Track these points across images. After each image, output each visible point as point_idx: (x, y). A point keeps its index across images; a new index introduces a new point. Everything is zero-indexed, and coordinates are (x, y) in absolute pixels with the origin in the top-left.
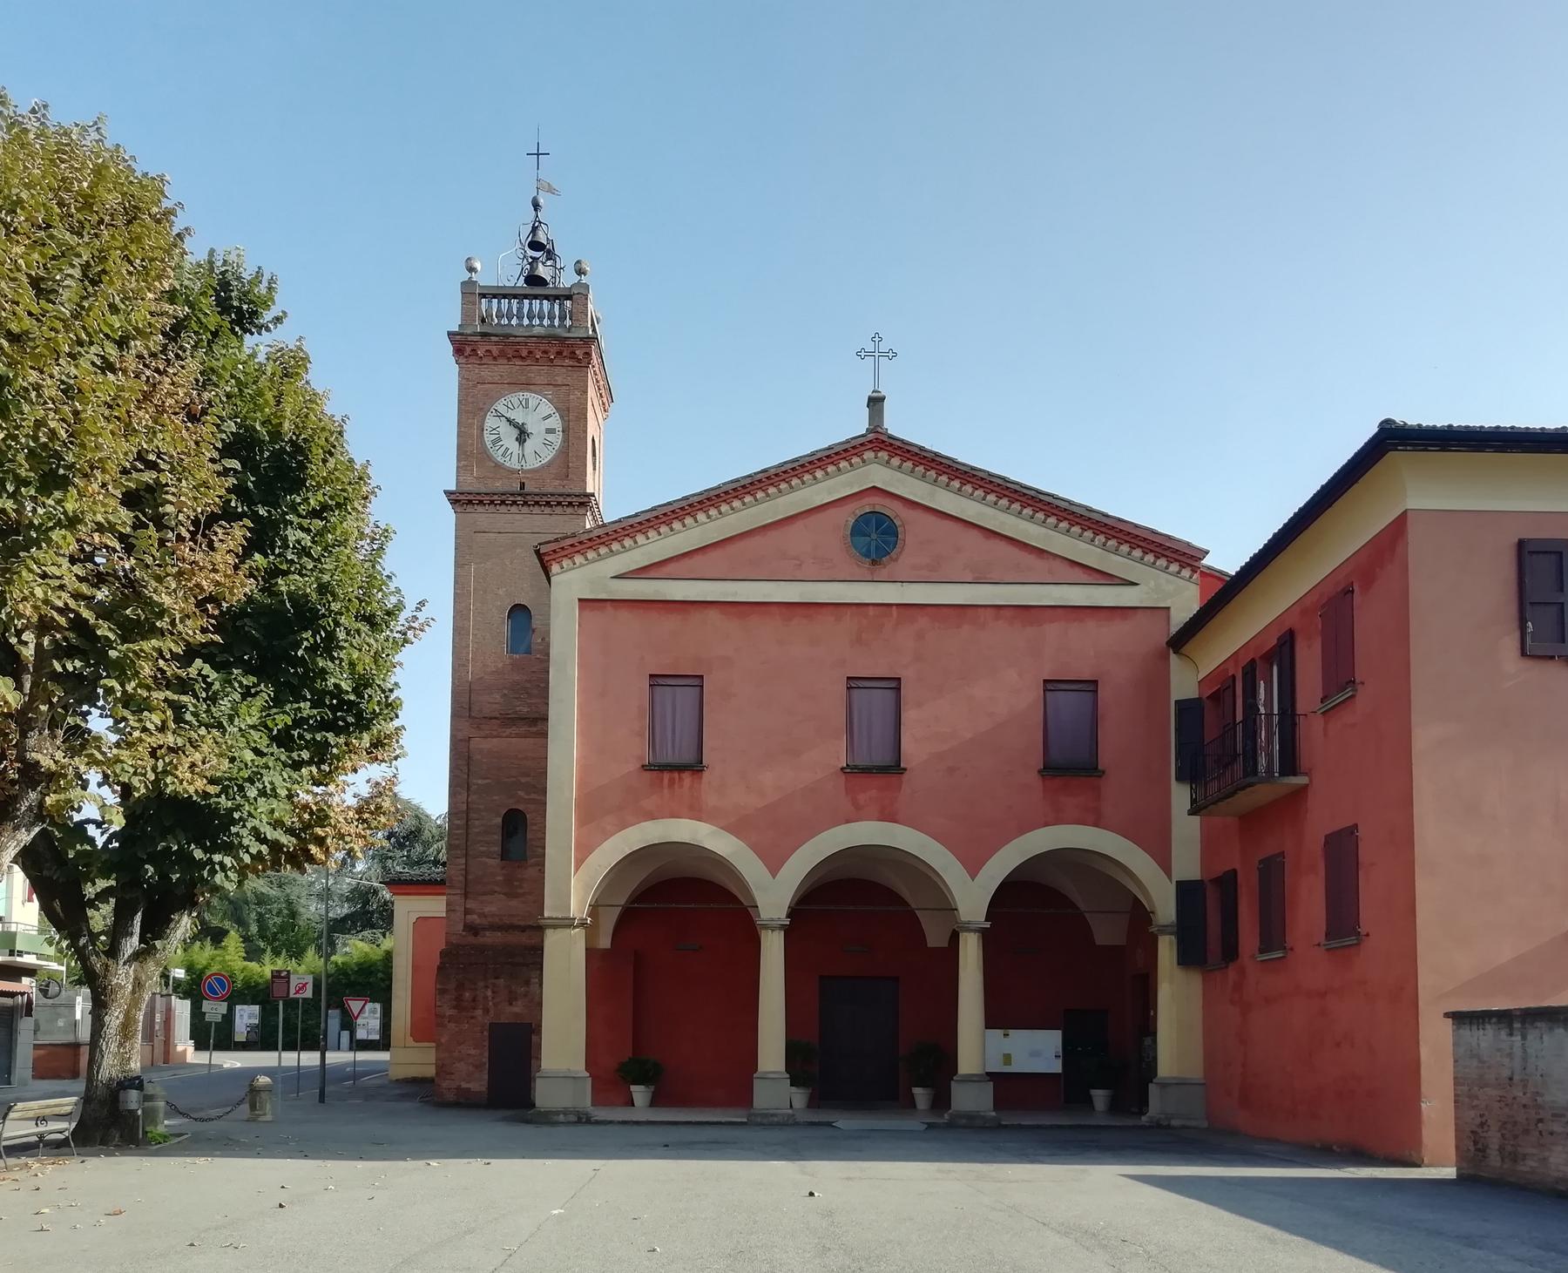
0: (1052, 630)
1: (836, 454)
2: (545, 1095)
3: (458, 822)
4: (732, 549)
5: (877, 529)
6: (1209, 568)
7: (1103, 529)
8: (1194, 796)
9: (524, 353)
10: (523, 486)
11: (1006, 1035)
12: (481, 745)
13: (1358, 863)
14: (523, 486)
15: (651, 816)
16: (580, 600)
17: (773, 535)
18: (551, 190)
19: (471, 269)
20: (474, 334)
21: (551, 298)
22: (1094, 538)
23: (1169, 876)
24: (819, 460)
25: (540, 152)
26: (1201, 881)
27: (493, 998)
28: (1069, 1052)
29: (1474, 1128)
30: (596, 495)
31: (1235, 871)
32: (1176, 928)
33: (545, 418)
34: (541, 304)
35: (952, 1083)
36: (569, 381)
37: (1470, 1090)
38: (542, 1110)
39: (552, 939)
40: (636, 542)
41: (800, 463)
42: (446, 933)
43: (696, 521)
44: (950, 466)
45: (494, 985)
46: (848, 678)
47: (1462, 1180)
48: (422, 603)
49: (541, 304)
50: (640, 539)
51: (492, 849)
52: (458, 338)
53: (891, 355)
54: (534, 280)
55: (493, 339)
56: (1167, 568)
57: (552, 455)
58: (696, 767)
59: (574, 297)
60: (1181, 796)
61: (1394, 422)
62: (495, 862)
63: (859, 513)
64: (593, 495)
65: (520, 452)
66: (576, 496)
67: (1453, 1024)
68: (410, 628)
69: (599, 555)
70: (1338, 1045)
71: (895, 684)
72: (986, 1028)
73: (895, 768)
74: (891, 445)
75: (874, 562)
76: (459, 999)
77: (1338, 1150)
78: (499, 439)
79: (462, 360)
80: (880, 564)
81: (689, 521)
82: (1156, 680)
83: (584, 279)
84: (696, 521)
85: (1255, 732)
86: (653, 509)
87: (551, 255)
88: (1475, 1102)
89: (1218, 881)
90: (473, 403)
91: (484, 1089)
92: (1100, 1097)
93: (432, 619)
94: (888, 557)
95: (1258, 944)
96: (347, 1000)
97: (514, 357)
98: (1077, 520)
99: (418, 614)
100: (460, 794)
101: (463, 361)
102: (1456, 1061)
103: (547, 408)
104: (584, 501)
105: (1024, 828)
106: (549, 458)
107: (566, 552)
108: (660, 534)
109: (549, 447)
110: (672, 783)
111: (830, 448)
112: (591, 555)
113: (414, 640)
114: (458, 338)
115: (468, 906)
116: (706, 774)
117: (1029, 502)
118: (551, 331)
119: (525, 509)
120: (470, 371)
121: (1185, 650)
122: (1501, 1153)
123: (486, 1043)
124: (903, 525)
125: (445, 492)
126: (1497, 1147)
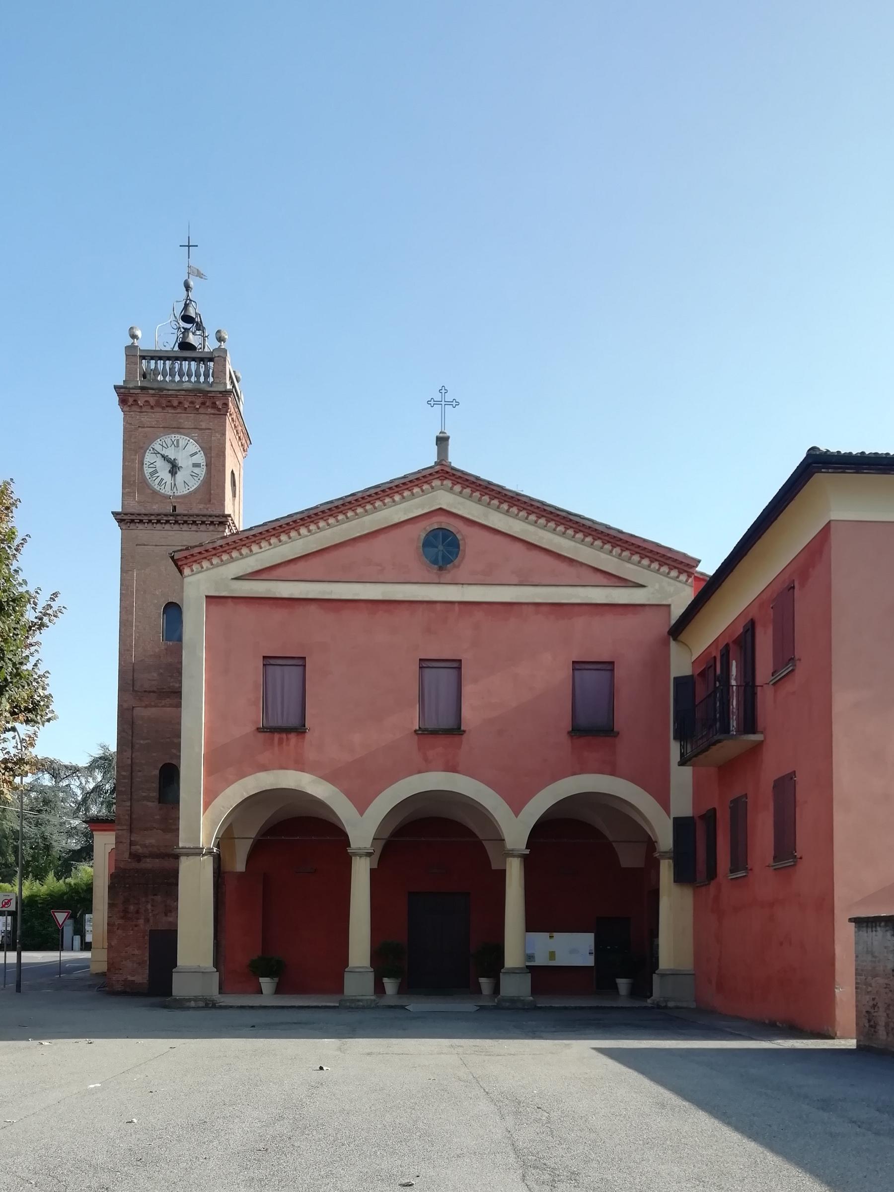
0: (579, 623)
1: (411, 481)
2: (180, 987)
3: (124, 773)
4: (327, 557)
5: (443, 543)
6: (702, 574)
7: (619, 543)
8: (682, 751)
9: (175, 403)
10: (174, 508)
11: (551, 937)
12: (140, 712)
13: (795, 802)
14: (174, 508)
15: (264, 768)
16: (207, 597)
17: (362, 546)
18: (199, 275)
19: (134, 336)
20: (136, 388)
21: (197, 360)
22: (612, 550)
23: (668, 813)
24: (397, 486)
25: (190, 244)
26: (693, 817)
27: (152, 910)
28: (599, 950)
29: (869, 1009)
30: (232, 516)
31: (714, 809)
32: (673, 854)
33: (192, 455)
34: (189, 365)
35: (501, 974)
36: (211, 425)
37: (866, 979)
38: (178, 998)
39: (186, 865)
40: (251, 551)
41: (382, 489)
42: (116, 860)
43: (299, 534)
44: (500, 492)
45: (153, 900)
46: (420, 660)
47: (861, 1049)
48: (55, 594)
49: (189, 365)
50: (255, 548)
51: (151, 795)
52: (122, 390)
53: (454, 403)
54: (185, 346)
55: (151, 392)
56: (668, 573)
57: (198, 484)
58: (300, 730)
59: (216, 358)
60: (675, 749)
61: (818, 449)
62: (153, 805)
63: (429, 529)
64: (229, 516)
65: (173, 482)
66: (216, 516)
67: (855, 927)
68: (45, 614)
69: (222, 561)
70: (781, 944)
71: (457, 665)
72: (526, 932)
73: (456, 731)
74: (454, 475)
75: (441, 569)
76: (126, 911)
77: (780, 1025)
78: (156, 472)
79: (127, 409)
80: (445, 570)
81: (293, 534)
82: (660, 661)
83: (223, 345)
84: (299, 534)
85: (729, 701)
86: (264, 524)
87: (200, 327)
88: (870, 989)
89: (702, 817)
90: (135, 442)
91: (145, 981)
92: (623, 984)
93: (63, 607)
94: (451, 564)
95: (730, 866)
96: (53, 912)
97: (167, 406)
98: (580, 528)
99: (52, 604)
100: (126, 751)
101: (127, 410)
102: (857, 957)
103: (193, 447)
104: (223, 520)
105: (555, 778)
106: (196, 486)
107: (195, 558)
108: (270, 544)
109: (195, 478)
110: (281, 741)
111: (405, 477)
112: (215, 561)
113: (49, 624)
114: (122, 390)
115: (132, 839)
116: (308, 736)
117: (562, 521)
118: (197, 386)
119: (176, 527)
120: (132, 417)
121: (681, 637)
122: (886, 1028)
123: (147, 946)
124: (463, 539)
125: (113, 513)
126: (883, 1024)
